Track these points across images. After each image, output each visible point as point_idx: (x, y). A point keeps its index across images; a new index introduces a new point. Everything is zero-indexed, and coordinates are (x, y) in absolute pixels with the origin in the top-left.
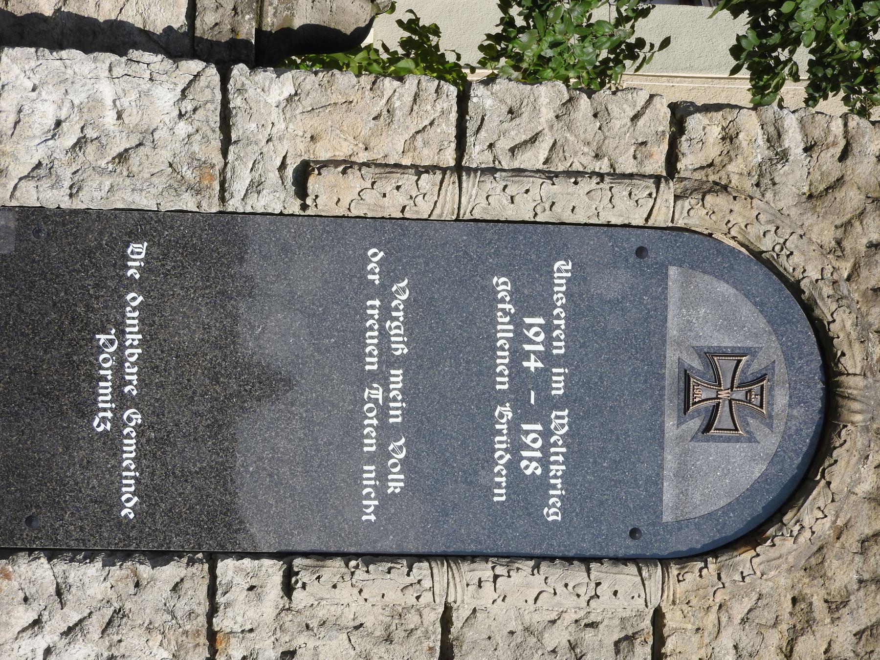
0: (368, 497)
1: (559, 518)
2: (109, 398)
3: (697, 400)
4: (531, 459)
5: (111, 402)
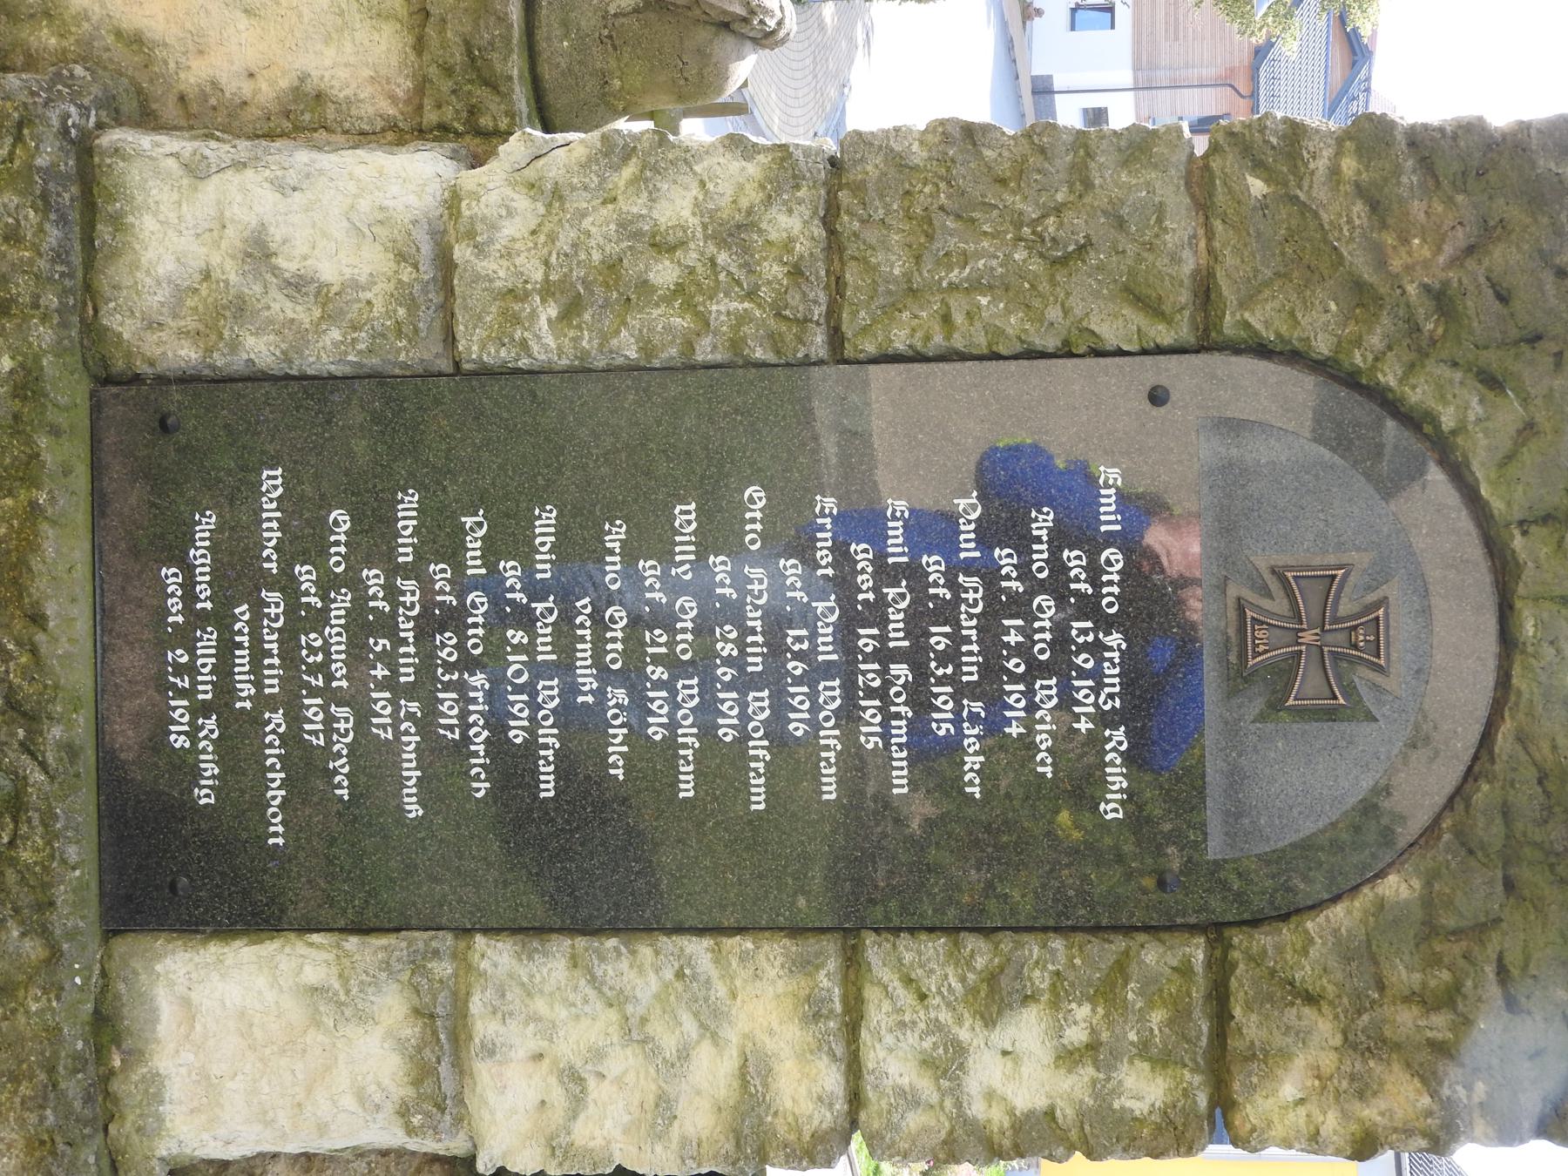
0: (272, 768)
1: (1120, 816)
2: (247, 668)
3: (1262, 648)
4: (179, 733)
5: (248, 673)
